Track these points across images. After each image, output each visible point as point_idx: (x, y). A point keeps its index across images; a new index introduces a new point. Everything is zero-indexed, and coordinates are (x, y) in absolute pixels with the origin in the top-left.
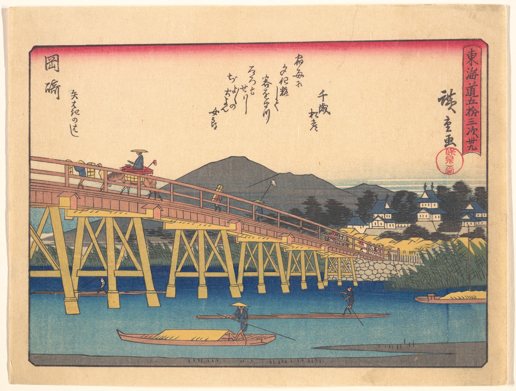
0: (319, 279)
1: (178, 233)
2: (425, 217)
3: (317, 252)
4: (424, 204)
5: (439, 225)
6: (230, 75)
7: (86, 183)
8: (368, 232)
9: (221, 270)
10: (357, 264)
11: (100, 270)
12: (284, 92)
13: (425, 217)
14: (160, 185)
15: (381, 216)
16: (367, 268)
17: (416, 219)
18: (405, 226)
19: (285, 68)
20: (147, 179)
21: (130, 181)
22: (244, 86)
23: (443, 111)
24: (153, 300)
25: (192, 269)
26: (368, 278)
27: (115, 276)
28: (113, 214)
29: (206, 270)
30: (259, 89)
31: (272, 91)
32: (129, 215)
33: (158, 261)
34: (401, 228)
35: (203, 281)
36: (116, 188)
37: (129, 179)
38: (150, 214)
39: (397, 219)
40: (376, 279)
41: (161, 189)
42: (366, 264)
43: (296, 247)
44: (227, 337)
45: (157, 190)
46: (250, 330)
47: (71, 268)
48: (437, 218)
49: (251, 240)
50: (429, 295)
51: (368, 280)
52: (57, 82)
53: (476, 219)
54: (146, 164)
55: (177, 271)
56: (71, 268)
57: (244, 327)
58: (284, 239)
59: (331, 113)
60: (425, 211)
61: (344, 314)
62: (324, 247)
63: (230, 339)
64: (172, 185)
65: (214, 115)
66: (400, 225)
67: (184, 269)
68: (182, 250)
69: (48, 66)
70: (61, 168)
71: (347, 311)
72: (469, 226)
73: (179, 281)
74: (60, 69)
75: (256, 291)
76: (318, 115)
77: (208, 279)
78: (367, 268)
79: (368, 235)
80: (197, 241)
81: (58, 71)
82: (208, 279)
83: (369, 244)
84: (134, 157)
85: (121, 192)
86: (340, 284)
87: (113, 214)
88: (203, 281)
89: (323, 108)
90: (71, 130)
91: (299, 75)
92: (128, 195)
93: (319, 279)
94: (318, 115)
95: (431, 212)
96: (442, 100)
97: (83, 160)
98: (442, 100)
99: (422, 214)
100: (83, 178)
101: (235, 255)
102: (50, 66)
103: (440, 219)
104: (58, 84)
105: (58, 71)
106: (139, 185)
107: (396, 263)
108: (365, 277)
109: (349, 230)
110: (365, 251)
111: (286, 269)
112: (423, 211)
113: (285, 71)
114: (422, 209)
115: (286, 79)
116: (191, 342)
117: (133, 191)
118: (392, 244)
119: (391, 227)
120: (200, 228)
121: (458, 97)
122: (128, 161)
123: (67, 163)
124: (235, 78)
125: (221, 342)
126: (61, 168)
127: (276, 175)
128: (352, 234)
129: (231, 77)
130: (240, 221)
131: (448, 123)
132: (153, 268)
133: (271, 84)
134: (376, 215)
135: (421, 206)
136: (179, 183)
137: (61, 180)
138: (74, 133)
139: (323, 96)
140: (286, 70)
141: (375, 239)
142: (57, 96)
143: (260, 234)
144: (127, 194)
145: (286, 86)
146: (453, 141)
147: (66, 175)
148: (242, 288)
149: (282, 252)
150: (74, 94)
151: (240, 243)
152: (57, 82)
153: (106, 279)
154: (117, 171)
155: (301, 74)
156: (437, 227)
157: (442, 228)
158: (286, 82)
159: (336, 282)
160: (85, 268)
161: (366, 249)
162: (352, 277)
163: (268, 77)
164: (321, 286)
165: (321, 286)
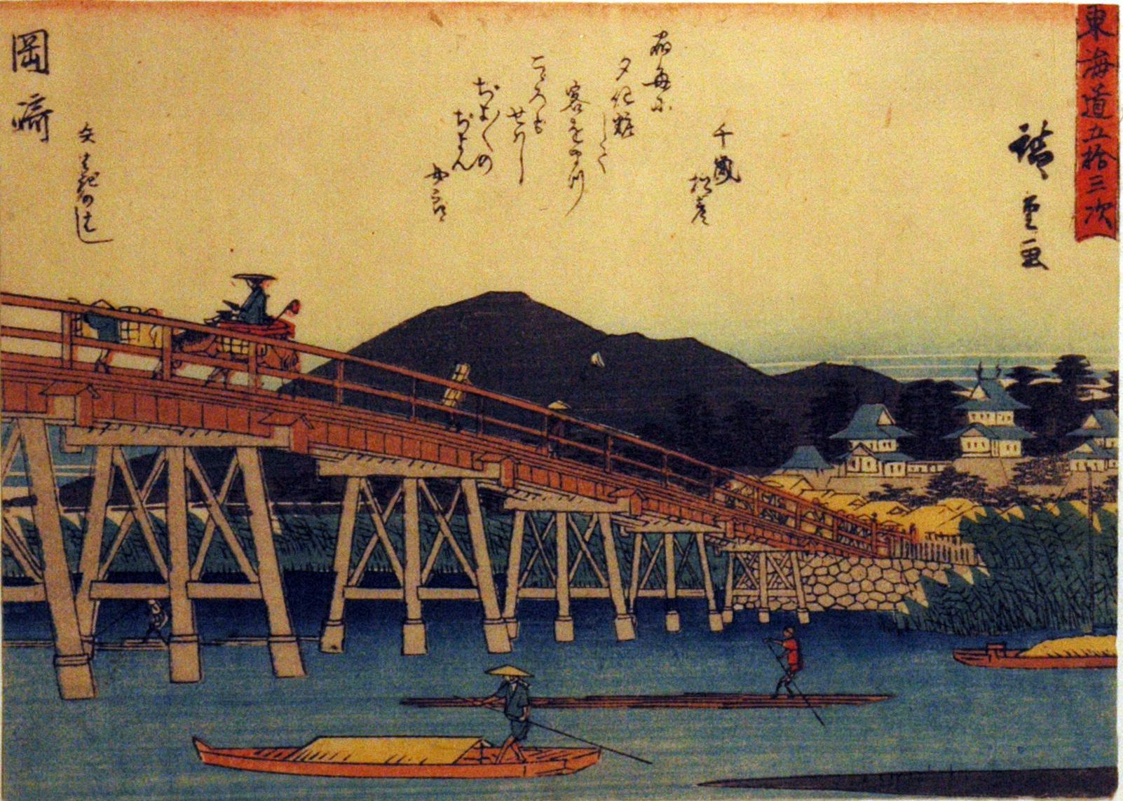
0: (712, 605)
1: (353, 487)
2: (980, 445)
3: (707, 538)
4: (978, 414)
5: (1015, 469)
6: (480, 83)
7: (121, 360)
8: (835, 484)
9: (465, 582)
10: (808, 568)
11: (147, 581)
12: (623, 126)
13: (980, 445)
14: (309, 363)
15: (869, 446)
16: (834, 579)
17: (953, 451)
18: (920, 469)
19: (626, 62)
20: (272, 346)
21: (231, 352)
22: (518, 110)
23: (1025, 176)
24: (287, 659)
25: (390, 580)
26: (835, 604)
27: (190, 596)
28: (186, 440)
29: (424, 581)
30: (557, 120)
31: (594, 122)
32: (226, 440)
33: (300, 562)
34: (916, 477)
35: (414, 611)
36: (198, 372)
37: (227, 348)
38: (282, 438)
39: (911, 449)
40: (859, 607)
41: (313, 372)
42: (837, 571)
43: (656, 524)
44: (477, 755)
45: (65, 352)
46: (536, 737)
47: (76, 579)
48: (1011, 449)
49: (540, 505)
50: (990, 647)
51: (836, 607)
52: (42, 99)
53: (882, 430)
54: (274, 308)
55: (350, 584)
56: (76, 579)
57: (522, 728)
58: (622, 505)
59: (1023, 123)
60: (978, 433)
61: (774, 696)
62: (497, 466)
63: (484, 761)
64: (336, 364)
65: (436, 183)
66: (917, 468)
67: (366, 582)
68: (362, 534)
69: (19, 59)
70: (50, 321)
71: (783, 690)
72: (1088, 469)
73: (352, 607)
74: (51, 69)
75: (551, 636)
76: (712, 185)
77: (427, 605)
78: (834, 579)
79: (836, 494)
80: (400, 507)
81: (46, 71)
82: (427, 605)
83: (840, 517)
84: (241, 293)
85: (208, 382)
86: (764, 618)
87: (186, 440)
88: (414, 611)
89: (723, 165)
90: (78, 225)
91: (661, 81)
92: (226, 389)
93: (712, 605)
94: (712, 185)
95: (992, 433)
96: (1017, 147)
97: (107, 300)
98: (1017, 147)
99: (972, 440)
100: (114, 346)
101: (498, 545)
102: (25, 57)
103: (1018, 453)
104: (45, 105)
105: (46, 71)
106: (258, 366)
107: (907, 564)
108: (827, 601)
109: (786, 481)
110: (828, 534)
111: (626, 583)
112: (973, 431)
113: (625, 70)
114: (973, 425)
115: (626, 91)
116: (385, 768)
117: (240, 379)
118: (896, 519)
119: (897, 472)
120: (407, 472)
121: (1064, 145)
122: (225, 302)
123: (70, 308)
124: (493, 89)
125: (463, 768)
126: (50, 321)
127: (597, 339)
128: (796, 491)
129: (484, 88)
130: (508, 457)
131: (1030, 205)
132: (290, 579)
133: (588, 103)
134: (855, 443)
135: (972, 420)
136: (357, 359)
137: (52, 350)
138: (83, 232)
139: (723, 134)
140: (629, 69)
141: (852, 504)
142: (42, 135)
143: (669, 518)
144: (223, 386)
145: (628, 108)
146: (1041, 258)
147: (71, 338)
148: (513, 629)
149: (617, 537)
150: (86, 135)
151: (512, 513)
152: (42, 99)
153: (166, 603)
154: (199, 329)
155: (665, 78)
156: (1011, 474)
157: (1022, 474)
158: (628, 98)
159: (756, 611)
160: (114, 577)
161: (831, 529)
162: (794, 599)
163: (579, 87)
164: (716, 623)
165: (716, 623)
